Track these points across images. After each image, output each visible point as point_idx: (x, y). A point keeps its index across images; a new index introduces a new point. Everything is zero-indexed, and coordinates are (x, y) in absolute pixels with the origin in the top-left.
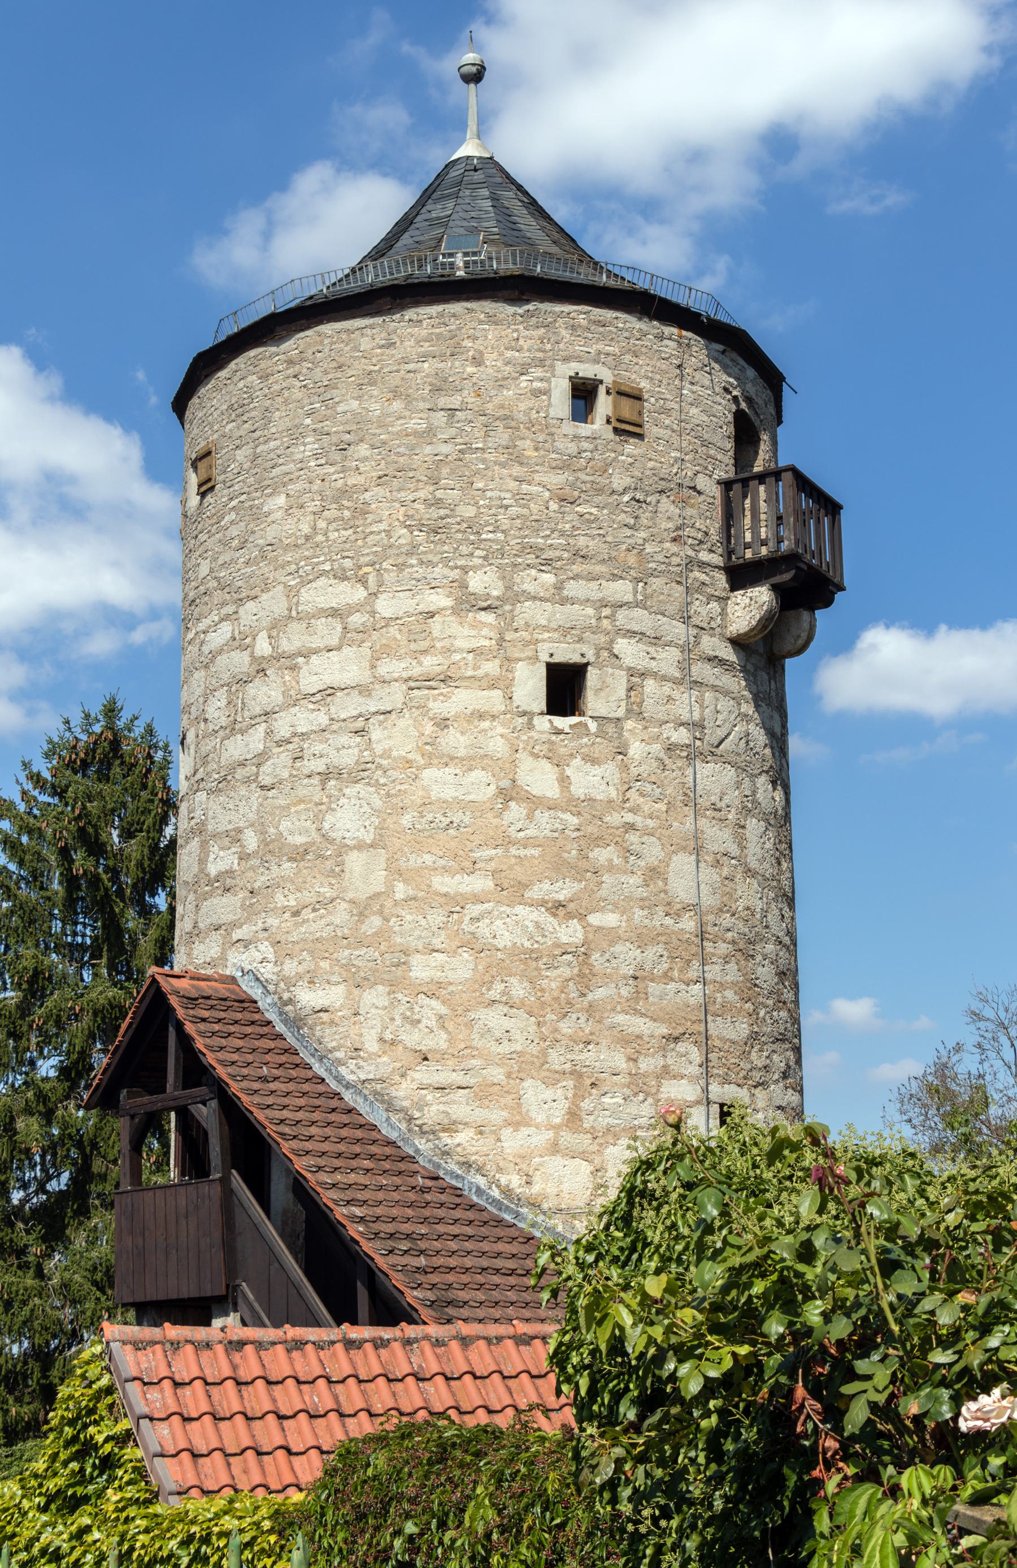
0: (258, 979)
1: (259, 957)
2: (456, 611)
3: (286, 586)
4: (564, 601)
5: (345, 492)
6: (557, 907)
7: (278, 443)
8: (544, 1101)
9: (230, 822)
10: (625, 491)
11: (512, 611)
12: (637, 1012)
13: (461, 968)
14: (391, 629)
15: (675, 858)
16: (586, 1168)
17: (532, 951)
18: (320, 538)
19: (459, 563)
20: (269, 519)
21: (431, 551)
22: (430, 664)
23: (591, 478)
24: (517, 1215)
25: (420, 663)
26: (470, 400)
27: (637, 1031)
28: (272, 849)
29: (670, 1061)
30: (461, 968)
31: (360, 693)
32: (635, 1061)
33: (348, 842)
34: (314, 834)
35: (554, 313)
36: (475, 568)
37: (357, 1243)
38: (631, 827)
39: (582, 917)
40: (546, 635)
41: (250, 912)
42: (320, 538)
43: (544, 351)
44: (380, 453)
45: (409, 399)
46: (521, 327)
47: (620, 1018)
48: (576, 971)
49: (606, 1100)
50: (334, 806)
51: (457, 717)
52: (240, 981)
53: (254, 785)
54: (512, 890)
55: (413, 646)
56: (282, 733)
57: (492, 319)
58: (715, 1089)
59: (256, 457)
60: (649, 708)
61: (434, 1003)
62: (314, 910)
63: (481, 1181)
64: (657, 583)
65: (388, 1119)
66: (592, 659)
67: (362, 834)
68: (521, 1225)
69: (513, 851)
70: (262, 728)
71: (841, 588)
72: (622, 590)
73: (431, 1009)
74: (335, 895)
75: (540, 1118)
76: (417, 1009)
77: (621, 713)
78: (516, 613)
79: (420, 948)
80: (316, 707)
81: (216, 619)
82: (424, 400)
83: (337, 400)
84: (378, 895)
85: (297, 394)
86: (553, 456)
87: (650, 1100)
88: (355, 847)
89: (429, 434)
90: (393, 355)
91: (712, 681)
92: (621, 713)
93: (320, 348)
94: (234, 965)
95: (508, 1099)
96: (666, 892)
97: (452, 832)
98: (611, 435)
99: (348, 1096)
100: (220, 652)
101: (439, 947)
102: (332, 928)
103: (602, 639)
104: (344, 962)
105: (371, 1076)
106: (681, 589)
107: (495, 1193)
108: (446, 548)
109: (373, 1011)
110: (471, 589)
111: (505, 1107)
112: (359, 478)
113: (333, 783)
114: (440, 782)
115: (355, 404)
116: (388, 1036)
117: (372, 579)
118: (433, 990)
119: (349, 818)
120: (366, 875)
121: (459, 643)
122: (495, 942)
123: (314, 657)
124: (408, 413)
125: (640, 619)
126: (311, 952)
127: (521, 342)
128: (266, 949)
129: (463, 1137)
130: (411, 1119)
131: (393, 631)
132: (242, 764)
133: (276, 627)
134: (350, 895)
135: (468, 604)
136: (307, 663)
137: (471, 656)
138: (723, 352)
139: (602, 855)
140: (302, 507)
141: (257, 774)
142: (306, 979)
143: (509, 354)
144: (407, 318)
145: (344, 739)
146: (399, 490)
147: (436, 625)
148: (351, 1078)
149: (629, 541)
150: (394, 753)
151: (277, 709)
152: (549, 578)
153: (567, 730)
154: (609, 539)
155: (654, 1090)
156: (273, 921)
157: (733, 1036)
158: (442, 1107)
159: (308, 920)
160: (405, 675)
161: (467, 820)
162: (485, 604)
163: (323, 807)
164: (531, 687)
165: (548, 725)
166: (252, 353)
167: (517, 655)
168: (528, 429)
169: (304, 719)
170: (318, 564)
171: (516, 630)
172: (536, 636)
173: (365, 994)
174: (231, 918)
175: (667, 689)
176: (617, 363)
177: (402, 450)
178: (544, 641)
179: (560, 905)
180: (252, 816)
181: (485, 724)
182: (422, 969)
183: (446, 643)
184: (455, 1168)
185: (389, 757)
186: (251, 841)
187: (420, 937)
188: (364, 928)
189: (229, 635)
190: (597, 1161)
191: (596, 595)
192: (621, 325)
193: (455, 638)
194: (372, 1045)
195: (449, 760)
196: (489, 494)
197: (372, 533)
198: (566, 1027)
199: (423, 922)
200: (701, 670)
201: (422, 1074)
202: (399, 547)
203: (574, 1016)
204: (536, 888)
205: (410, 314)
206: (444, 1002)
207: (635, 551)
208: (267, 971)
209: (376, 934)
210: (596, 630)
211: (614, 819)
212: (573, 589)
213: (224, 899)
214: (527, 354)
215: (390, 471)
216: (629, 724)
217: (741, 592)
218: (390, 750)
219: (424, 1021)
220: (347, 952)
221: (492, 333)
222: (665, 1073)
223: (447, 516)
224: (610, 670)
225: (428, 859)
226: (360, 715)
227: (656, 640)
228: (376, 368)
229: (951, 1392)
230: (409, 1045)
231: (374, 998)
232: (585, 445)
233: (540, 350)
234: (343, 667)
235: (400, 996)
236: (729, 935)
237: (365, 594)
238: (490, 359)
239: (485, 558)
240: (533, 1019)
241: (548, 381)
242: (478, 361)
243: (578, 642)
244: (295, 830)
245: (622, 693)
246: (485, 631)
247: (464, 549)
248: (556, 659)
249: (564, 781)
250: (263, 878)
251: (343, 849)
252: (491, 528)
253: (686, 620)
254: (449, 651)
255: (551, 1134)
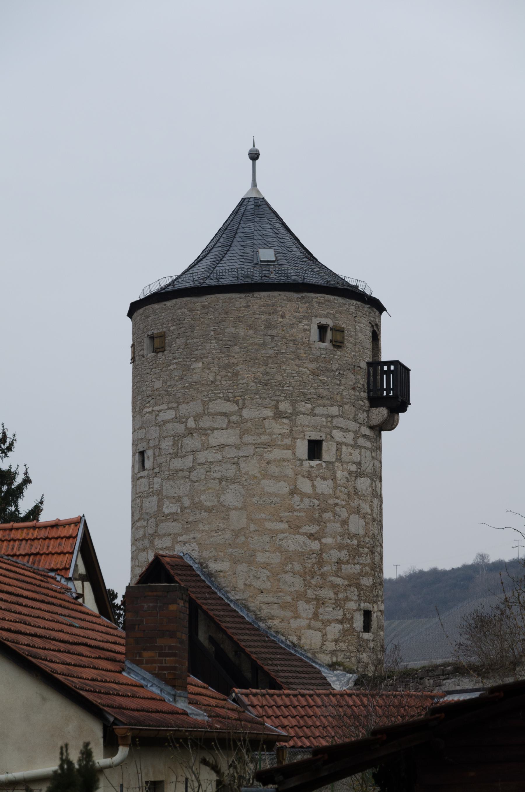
0: (191, 557)
1: (191, 548)
2: (274, 418)
3: (202, 400)
4: (315, 415)
5: (228, 366)
6: (311, 536)
7: (198, 340)
8: (305, 609)
9: (175, 493)
10: (337, 370)
11: (295, 419)
12: (338, 576)
13: (276, 558)
14: (248, 423)
15: (351, 516)
16: (320, 634)
17: (302, 552)
18: (218, 383)
19: (276, 399)
20: (195, 371)
21: (264, 393)
22: (264, 438)
23: (325, 365)
24: (296, 651)
25: (260, 438)
26: (280, 332)
27: (338, 583)
28: (196, 506)
29: (348, 594)
30: (276, 558)
31: (236, 448)
32: (337, 594)
33: (231, 507)
34: (216, 502)
35: (312, 297)
36: (281, 401)
37: (256, 661)
38: (336, 504)
39: (319, 540)
40: (308, 429)
41: (187, 531)
42: (218, 383)
43: (308, 313)
44: (244, 351)
45: (256, 331)
46: (299, 303)
47: (332, 578)
48: (317, 560)
49: (326, 609)
50: (225, 492)
51: (274, 461)
52: (183, 557)
53: (187, 480)
54: (295, 528)
55: (257, 431)
56: (201, 460)
57: (289, 299)
58: (362, 605)
59: (187, 344)
60: (345, 457)
61: (265, 571)
62: (216, 532)
63: (283, 638)
64: (347, 407)
65: (247, 614)
66: (324, 439)
67: (236, 504)
68: (298, 655)
69: (295, 514)
70: (191, 457)
71: (410, 404)
72: (335, 410)
73: (264, 574)
74: (225, 527)
75: (304, 615)
76: (259, 573)
77: (334, 460)
78: (297, 419)
79: (260, 549)
80: (216, 451)
81: (166, 407)
82: (262, 331)
83: (225, 326)
84: (243, 529)
85: (207, 322)
86: (311, 356)
87: (342, 609)
88: (234, 509)
89: (264, 345)
90: (249, 311)
91: (364, 445)
92: (334, 460)
93: (218, 304)
94: (178, 551)
95: (293, 608)
96: (348, 530)
97: (272, 505)
98: (332, 348)
99: (232, 606)
100: (169, 421)
101: (268, 549)
102: (224, 540)
103: (328, 430)
104: (230, 553)
105: (241, 598)
106: (354, 408)
107: (288, 643)
108: (270, 392)
109: (241, 573)
110: (280, 409)
111: (292, 611)
112: (235, 360)
113: (224, 483)
114: (269, 486)
115: (233, 330)
116: (247, 583)
117: (240, 402)
118: (266, 566)
119: (231, 497)
120: (237, 519)
121: (276, 431)
122: (288, 548)
123: (215, 431)
124: (255, 336)
125: (340, 422)
126: (215, 549)
127: (300, 309)
128: (194, 546)
129: (276, 622)
130: (256, 615)
131: (249, 424)
132: (182, 470)
133: (197, 417)
134: (232, 528)
135: (279, 415)
136: (213, 433)
137: (280, 436)
138: (369, 308)
139: (327, 515)
140: (210, 369)
141: (189, 476)
142: (213, 559)
143: (295, 314)
144: (255, 296)
145: (229, 466)
146: (252, 367)
147: (266, 423)
148: (233, 598)
149: (338, 390)
150: (250, 473)
151: (199, 450)
152: (309, 406)
153: (315, 467)
154: (331, 390)
155: (343, 605)
156: (198, 535)
157: (368, 585)
158: (268, 611)
159: (214, 536)
160: (254, 442)
161: (278, 501)
162: (285, 416)
163: (220, 492)
164: (302, 449)
165: (308, 465)
166: (185, 299)
167: (297, 437)
168: (302, 345)
169: (211, 456)
170: (217, 393)
171: (297, 427)
172: (305, 429)
173: (238, 566)
174: (176, 532)
175: (350, 449)
176: (334, 317)
177: (253, 351)
178: (307, 431)
179: (312, 535)
180: (187, 492)
181: (286, 464)
182: (261, 558)
183: (270, 430)
184: (274, 634)
185: (248, 474)
186: (187, 502)
187: (260, 546)
188: (238, 541)
189: (174, 416)
190: (324, 631)
191: (326, 413)
192: (336, 302)
193: (274, 429)
194: (241, 586)
195: (272, 477)
196: (287, 371)
197: (240, 383)
198: (314, 582)
199: (261, 540)
200: (361, 441)
201: (261, 598)
202: (251, 390)
203: (316, 577)
204: (303, 528)
205: (257, 294)
206: (269, 571)
207: (340, 395)
208: (195, 555)
209: (243, 543)
210: (325, 427)
211: (331, 501)
212: (319, 410)
213: (173, 524)
214: (302, 314)
215: (248, 359)
216: (337, 464)
217: (375, 408)
218: (248, 472)
219: (262, 578)
220: (230, 550)
221: (289, 305)
222: (347, 599)
223: (271, 379)
224: (331, 443)
225: (263, 516)
226: (236, 457)
227: (346, 430)
228: (242, 315)
229: (218, 778)
230: (256, 587)
231: (242, 568)
232: (323, 352)
233: (306, 313)
234: (230, 437)
235: (252, 568)
236: (367, 545)
237: (238, 408)
238: (288, 315)
239: (285, 397)
240: (302, 578)
241: (310, 325)
242: (283, 316)
243: (319, 432)
244: (207, 499)
245: (334, 451)
246: (285, 427)
247: (278, 393)
248: (312, 438)
249: (314, 486)
250: (192, 518)
251: (229, 509)
252: (288, 385)
253: (355, 421)
254: (270, 434)
255: (308, 621)
